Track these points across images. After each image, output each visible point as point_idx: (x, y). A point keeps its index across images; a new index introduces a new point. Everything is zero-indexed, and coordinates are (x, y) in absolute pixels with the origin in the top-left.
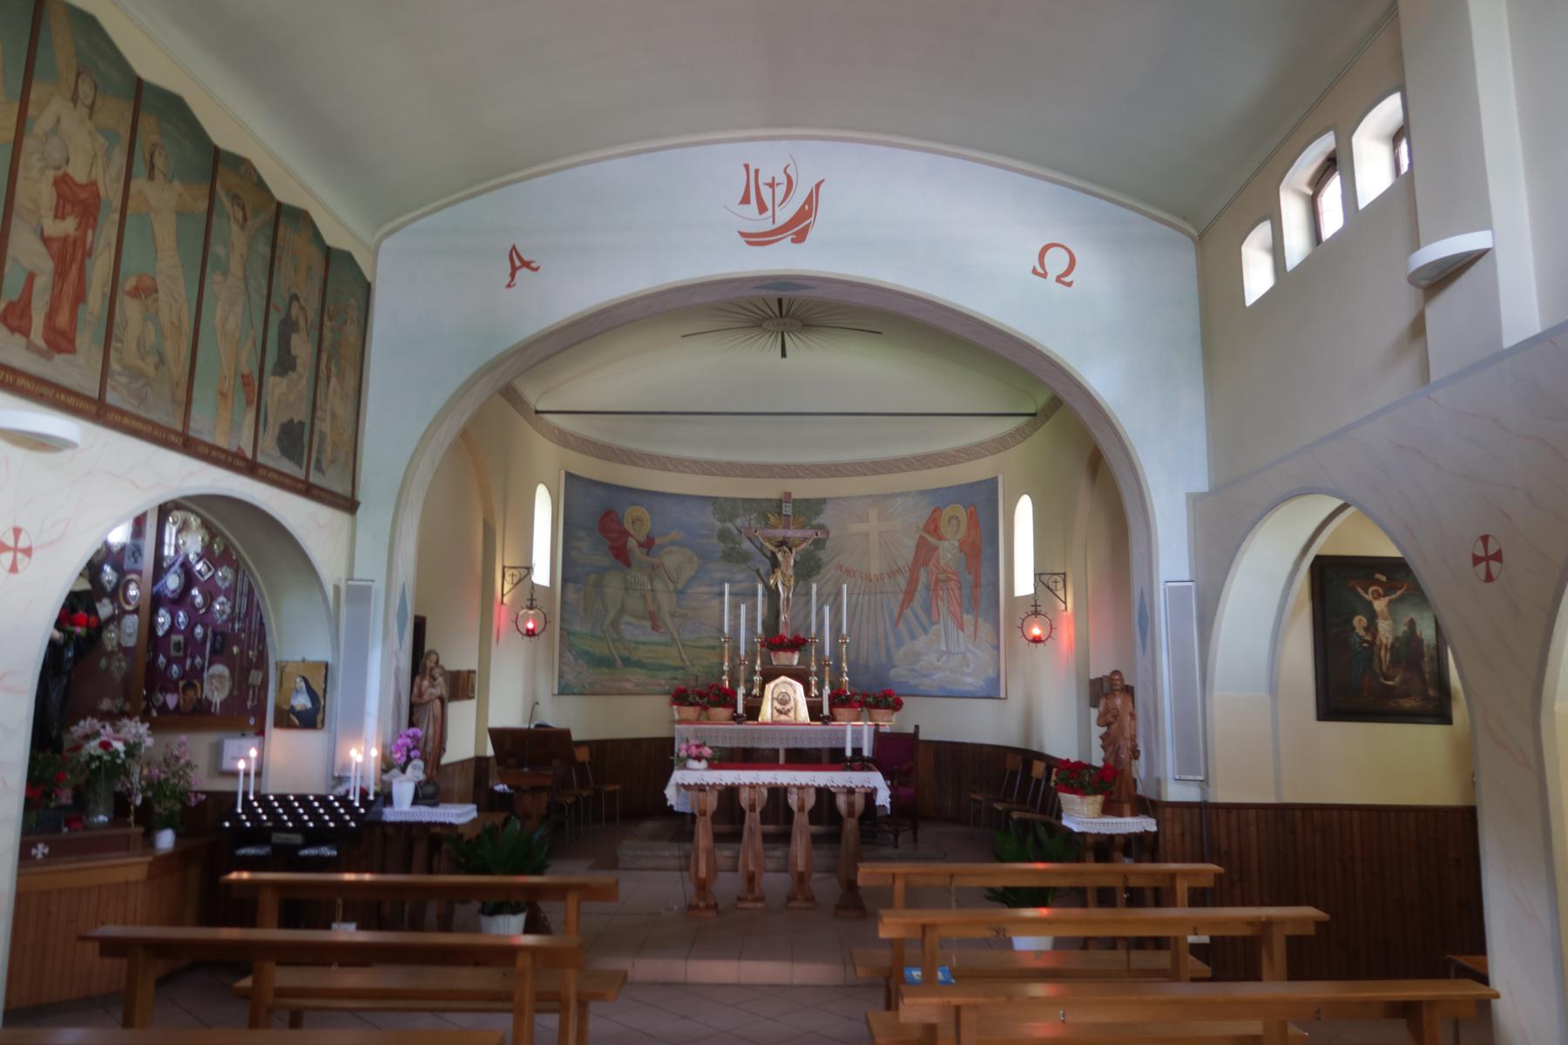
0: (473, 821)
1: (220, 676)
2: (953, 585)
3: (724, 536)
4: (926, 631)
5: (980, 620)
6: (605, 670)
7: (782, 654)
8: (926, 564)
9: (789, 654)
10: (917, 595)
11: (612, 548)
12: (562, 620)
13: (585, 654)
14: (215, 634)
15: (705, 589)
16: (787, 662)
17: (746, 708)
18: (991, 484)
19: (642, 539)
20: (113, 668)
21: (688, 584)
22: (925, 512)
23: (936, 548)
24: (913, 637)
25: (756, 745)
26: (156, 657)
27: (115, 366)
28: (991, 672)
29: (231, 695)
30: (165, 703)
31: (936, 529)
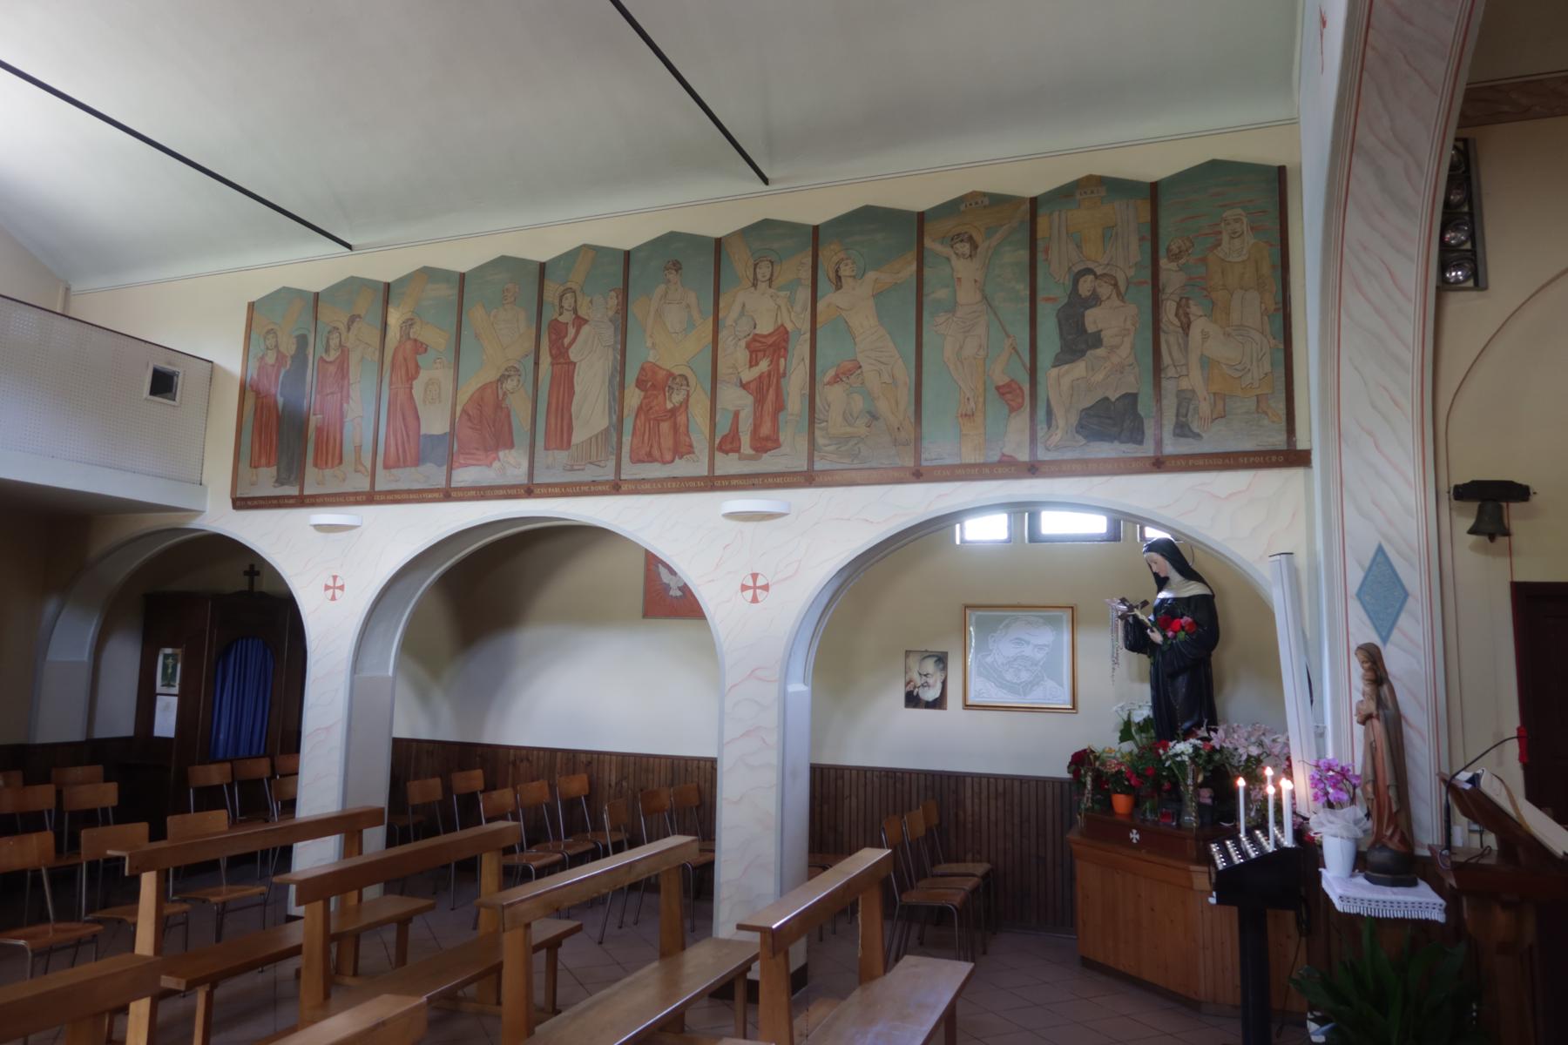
1: (926, 685)
27: (820, 441)
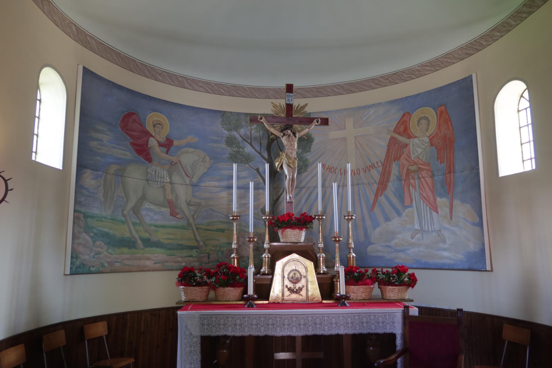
2: (424, 173)
3: (230, 141)
4: (399, 214)
5: (456, 202)
6: (125, 250)
7: (289, 231)
8: (397, 158)
9: (297, 231)
10: (390, 185)
11: (133, 144)
12: (76, 202)
13: (105, 236)
15: (216, 183)
16: (294, 240)
17: (257, 287)
18: (465, 87)
19: (162, 140)
21: (201, 180)
22: (395, 116)
23: (406, 145)
24: (387, 219)
25: (271, 333)
28: (473, 247)
31: (406, 129)
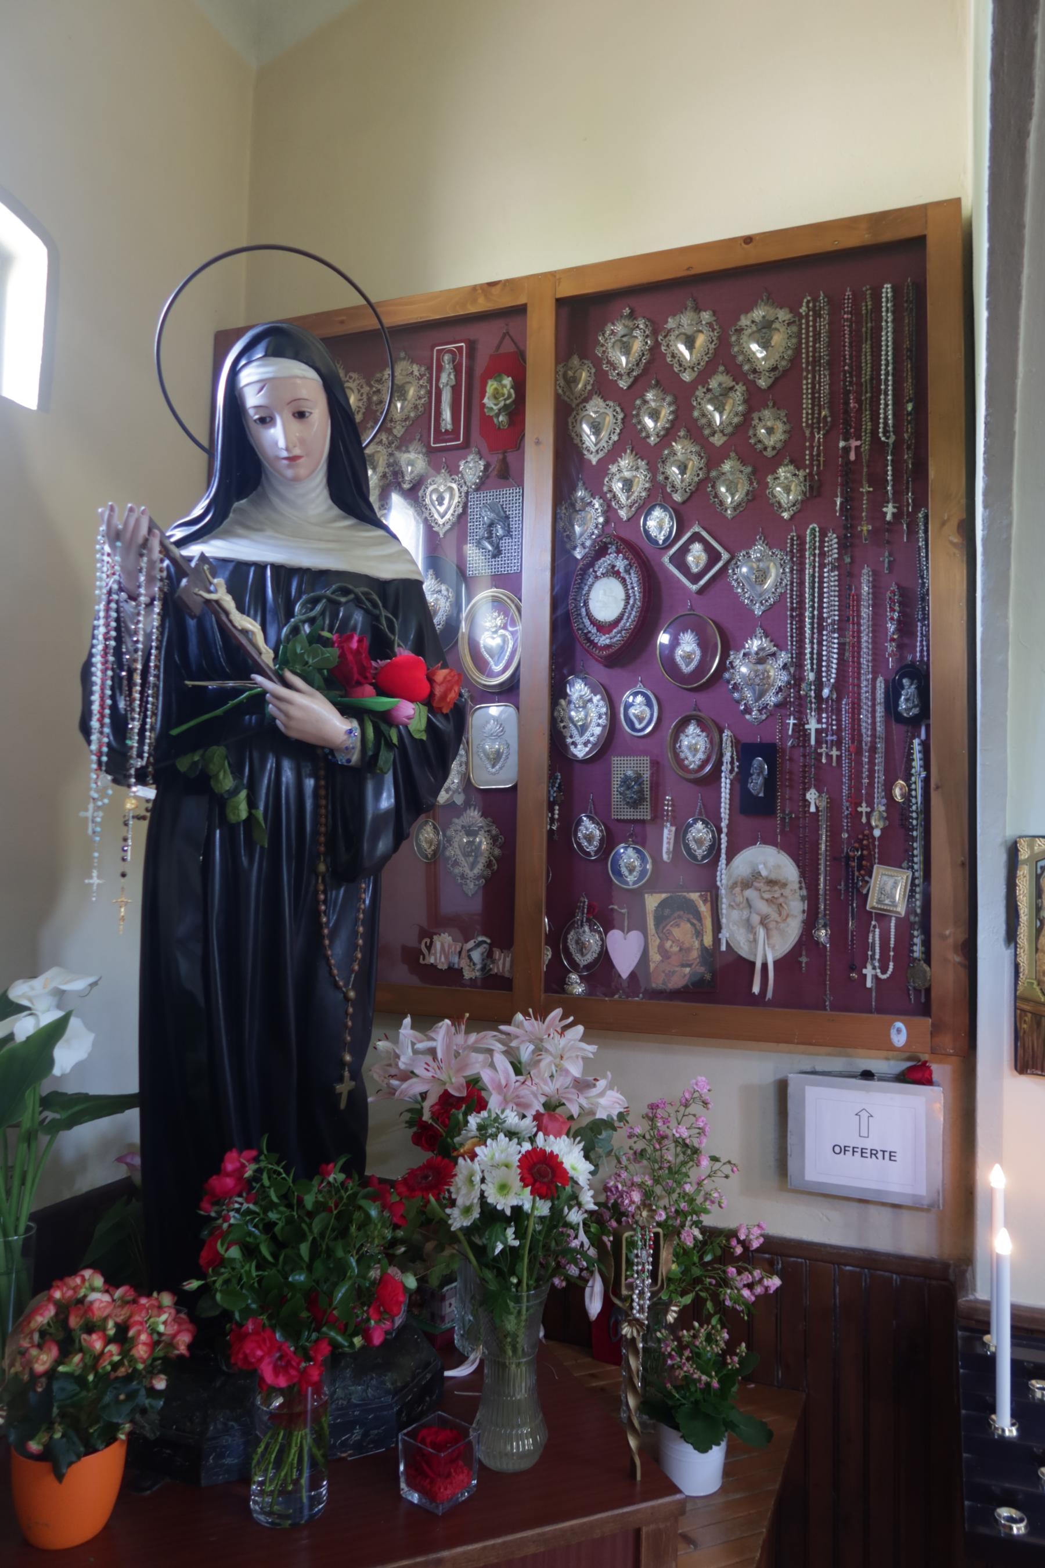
0: (95, 1044)
14: (746, 752)
20: (453, 852)
26: (569, 825)
29: (806, 940)
30: (604, 957)
